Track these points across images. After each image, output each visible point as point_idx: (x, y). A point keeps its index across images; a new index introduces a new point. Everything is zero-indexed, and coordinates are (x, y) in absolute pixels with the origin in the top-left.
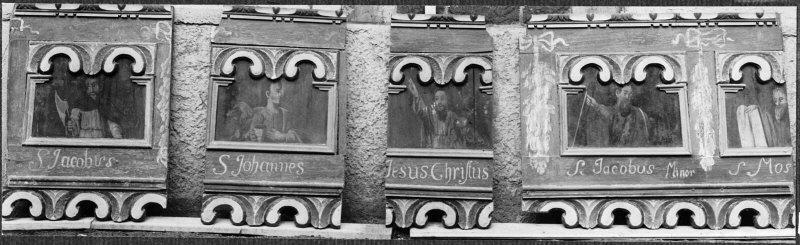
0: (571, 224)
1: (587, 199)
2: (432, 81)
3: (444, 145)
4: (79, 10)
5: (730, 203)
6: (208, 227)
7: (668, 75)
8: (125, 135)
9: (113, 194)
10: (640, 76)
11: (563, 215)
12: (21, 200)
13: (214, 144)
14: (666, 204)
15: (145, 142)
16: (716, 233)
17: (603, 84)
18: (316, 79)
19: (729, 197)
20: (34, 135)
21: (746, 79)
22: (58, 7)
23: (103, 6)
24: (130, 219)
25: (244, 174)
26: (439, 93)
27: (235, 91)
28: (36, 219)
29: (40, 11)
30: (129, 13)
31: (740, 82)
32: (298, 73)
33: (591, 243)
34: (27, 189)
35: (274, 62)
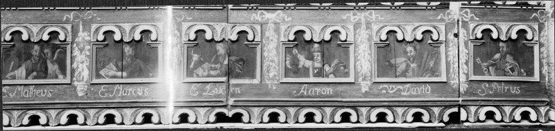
0: (391, 121)
1: (14, 110)
2: (29, 40)
3: (414, 76)
4: (295, 7)
5: (299, 109)
6: (247, 125)
7: (529, 36)
8: (527, 75)
9: (394, 108)
10: (514, 36)
11: (279, 117)
12: (237, 113)
13: (95, 81)
14: (299, 109)
15: (351, 79)
16: (327, 125)
17: (24, 41)
18: (249, 41)
19: (405, 106)
20: (474, 75)
21: (485, 37)
22: (393, 4)
23: (419, 3)
24: (479, 121)
25: (123, 97)
26: (409, 48)
27: (387, 48)
28: (43, 125)
29: (419, 6)
30: (432, 7)
31: (481, 39)
32: (331, 38)
33: (486, 130)
34: (348, 107)
35: (128, 31)
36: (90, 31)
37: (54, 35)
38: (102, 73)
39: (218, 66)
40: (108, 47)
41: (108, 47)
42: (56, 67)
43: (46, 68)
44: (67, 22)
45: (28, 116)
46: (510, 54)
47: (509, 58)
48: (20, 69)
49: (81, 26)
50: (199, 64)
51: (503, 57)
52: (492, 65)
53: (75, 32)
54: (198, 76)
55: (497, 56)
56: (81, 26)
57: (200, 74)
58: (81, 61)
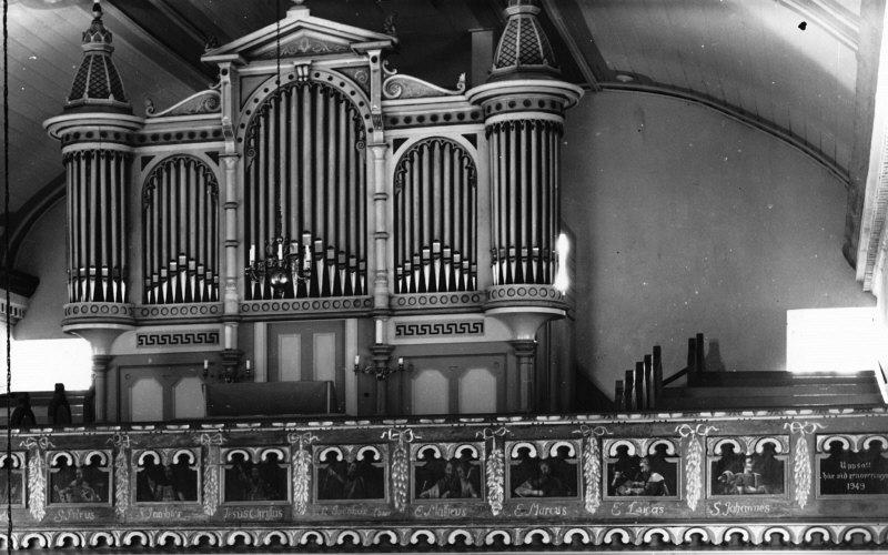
23: (274, 424)
36: (503, 448)
37: (467, 453)
38: (517, 492)
39: (642, 483)
40: (624, 471)
41: (624, 471)
42: (469, 485)
43: (460, 487)
44: (480, 439)
45: (269, 536)
46: (87, 481)
47: (85, 485)
48: (433, 489)
49: (494, 444)
50: (621, 482)
51: (79, 483)
52: (68, 492)
53: (489, 452)
54: (620, 495)
55: (74, 483)
56: (494, 444)
57: (622, 492)
58: (497, 486)
